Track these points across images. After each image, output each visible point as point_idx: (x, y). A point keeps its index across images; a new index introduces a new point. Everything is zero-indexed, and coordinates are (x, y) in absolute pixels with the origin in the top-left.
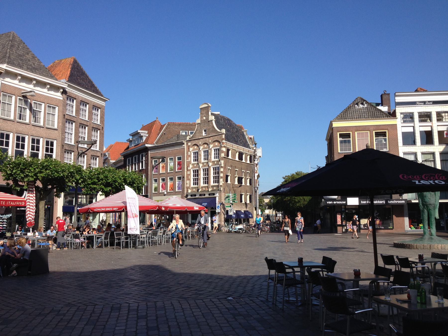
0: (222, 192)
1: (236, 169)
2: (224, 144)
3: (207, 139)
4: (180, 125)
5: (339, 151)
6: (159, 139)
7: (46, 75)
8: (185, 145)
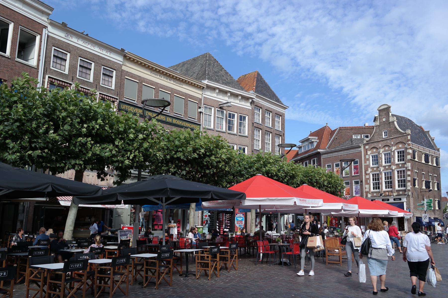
0: (411, 196)
1: (423, 173)
2: (410, 146)
3: (389, 141)
4: (352, 129)
6: (331, 144)
7: (238, 87)
8: (362, 149)
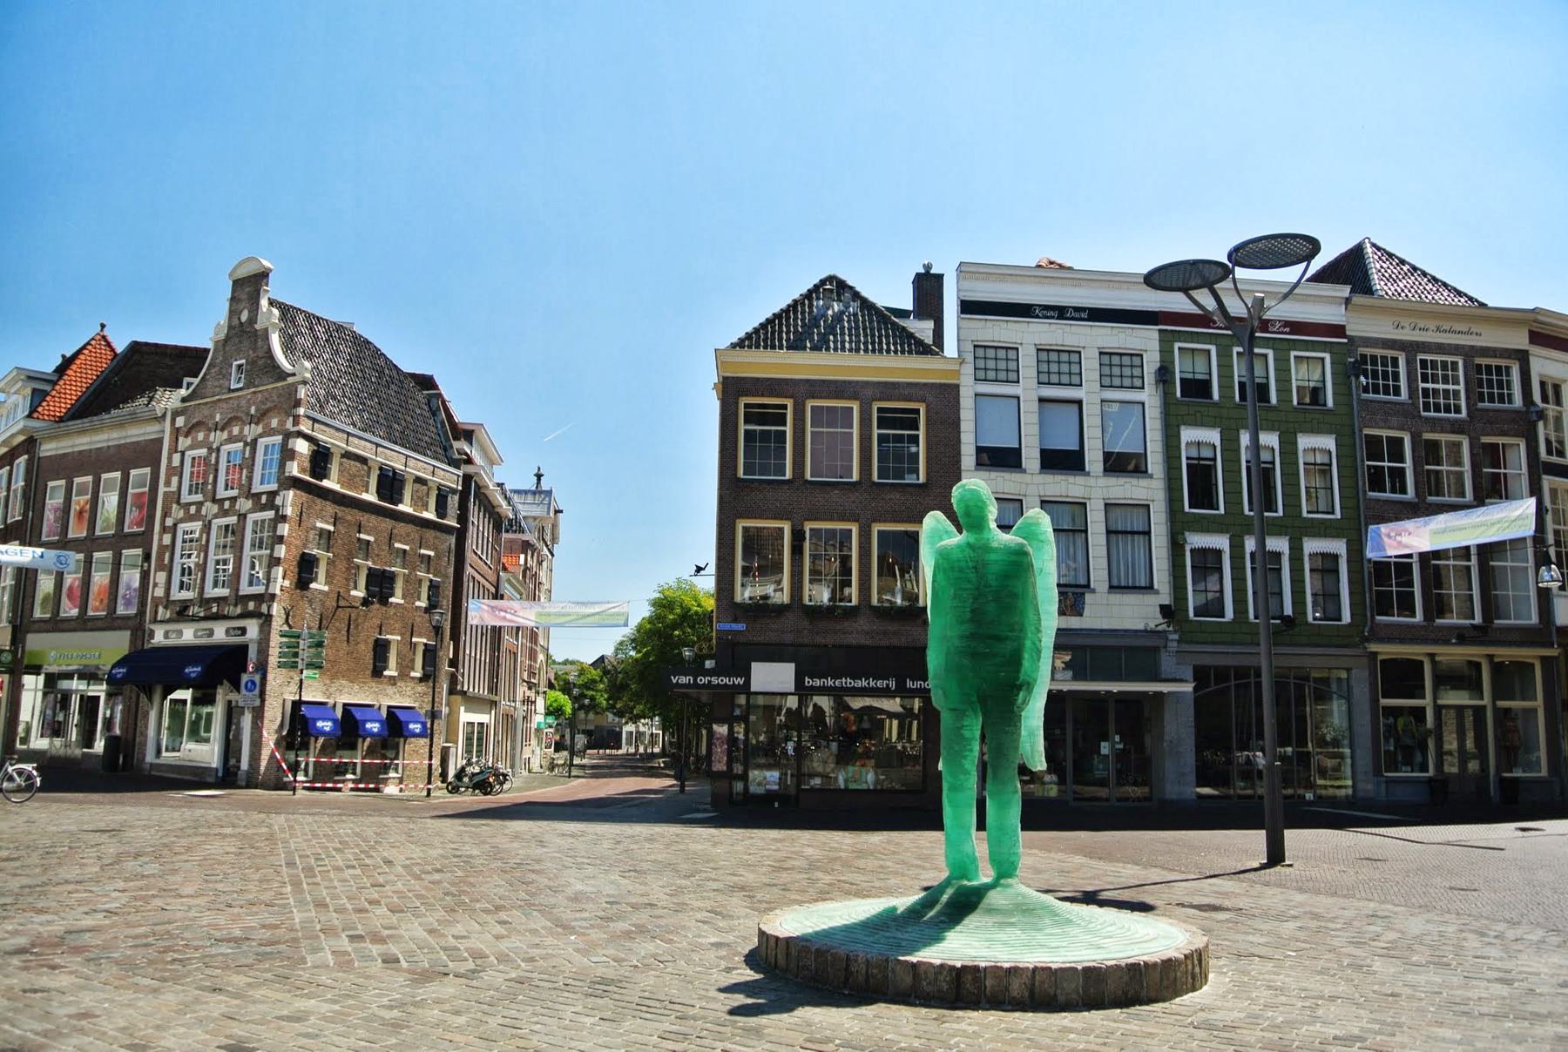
5: (741, 474)
